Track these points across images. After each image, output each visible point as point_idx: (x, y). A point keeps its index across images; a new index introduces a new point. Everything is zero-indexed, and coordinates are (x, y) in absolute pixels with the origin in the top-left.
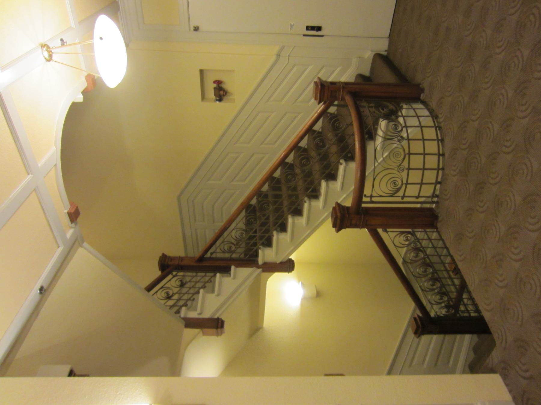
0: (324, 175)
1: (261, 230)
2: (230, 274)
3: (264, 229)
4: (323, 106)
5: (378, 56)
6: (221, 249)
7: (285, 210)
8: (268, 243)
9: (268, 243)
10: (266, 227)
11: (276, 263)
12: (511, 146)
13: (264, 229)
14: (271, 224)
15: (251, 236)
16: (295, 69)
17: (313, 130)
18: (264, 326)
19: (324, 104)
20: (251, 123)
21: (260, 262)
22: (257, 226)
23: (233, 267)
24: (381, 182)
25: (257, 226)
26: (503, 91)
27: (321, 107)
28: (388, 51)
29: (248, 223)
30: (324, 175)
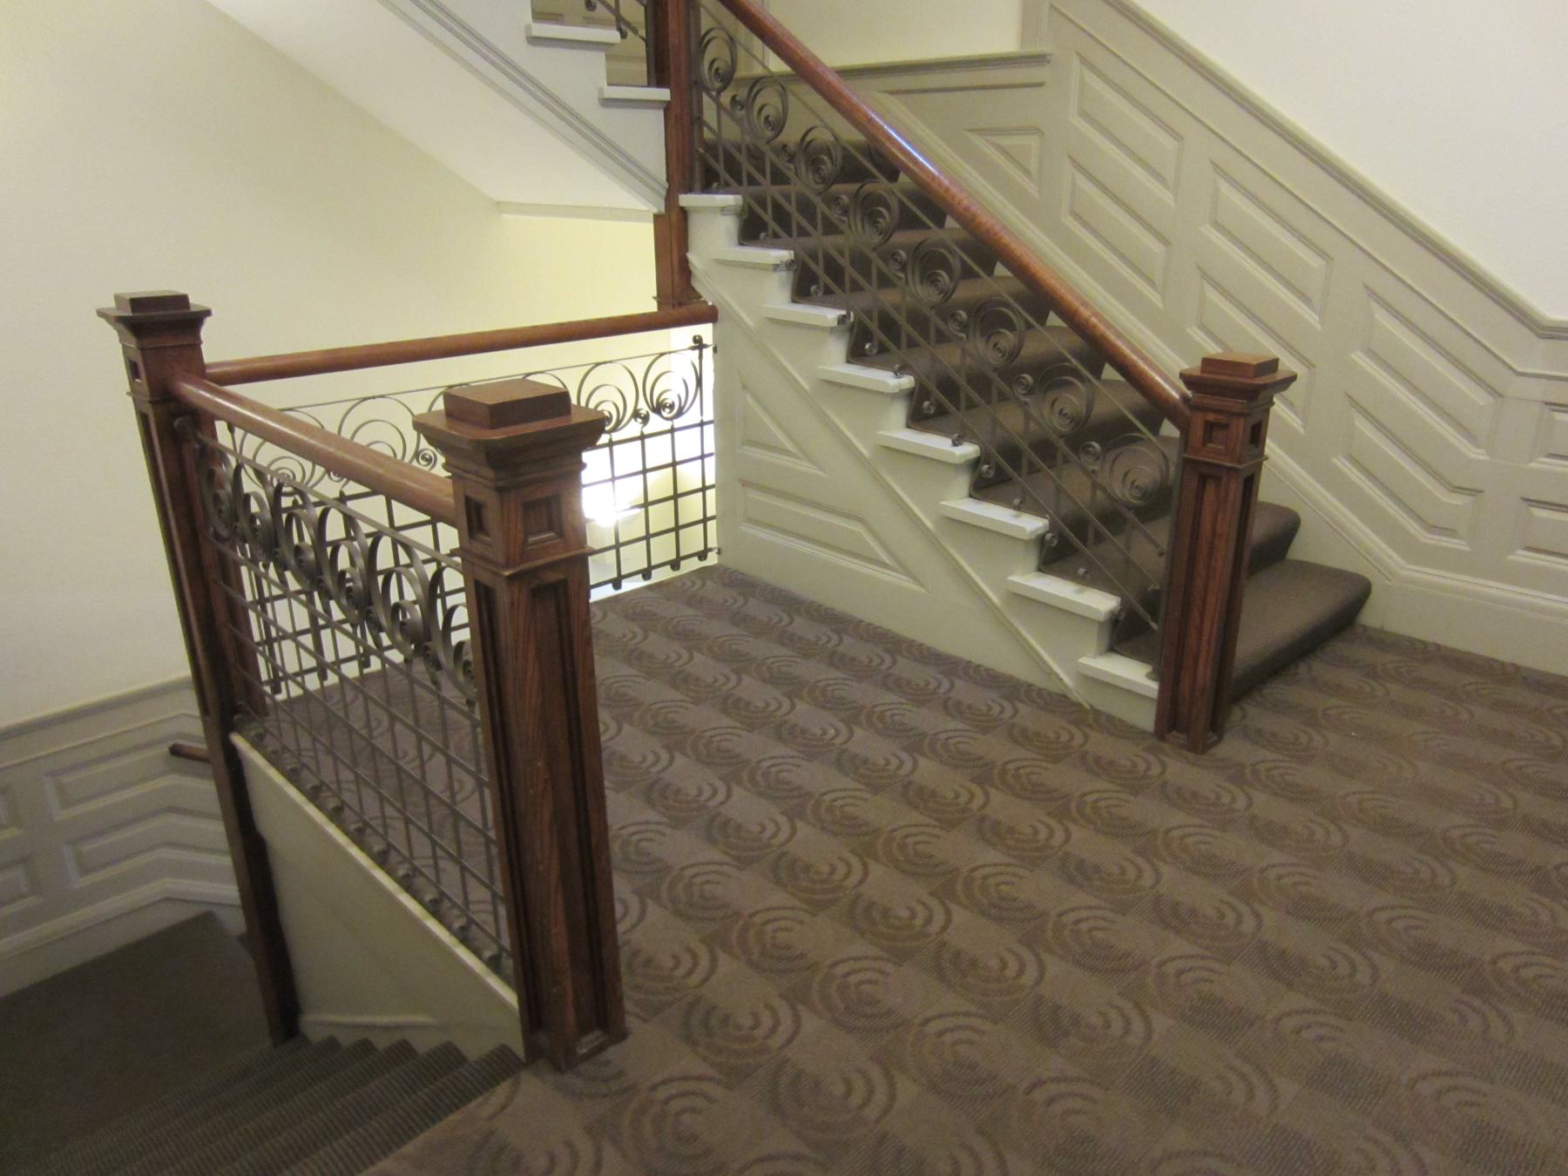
0: (1141, 610)
1: (788, 198)
2: (649, 85)
3: (797, 217)
4: (1176, 395)
5: (1359, 593)
6: (710, 30)
7: (864, 300)
8: (751, 230)
9: (751, 230)
10: (742, 158)
11: (687, 250)
12: (1230, 792)
13: (797, 217)
14: (821, 241)
15: (814, 207)
16: (1315, 262)
17: (1103, 365)
18: (504, 216)
19: (1185, 398)
20: (1119, 90)
21: (686, 200)
22: (803, 183)
23: (664, 94)
24: (399, 436)
25: (803, 183)
26: (1262, 767)
27: (1174, 391)
28: (1385, 641)
29: (810, 153)
30: (1141, 610)
